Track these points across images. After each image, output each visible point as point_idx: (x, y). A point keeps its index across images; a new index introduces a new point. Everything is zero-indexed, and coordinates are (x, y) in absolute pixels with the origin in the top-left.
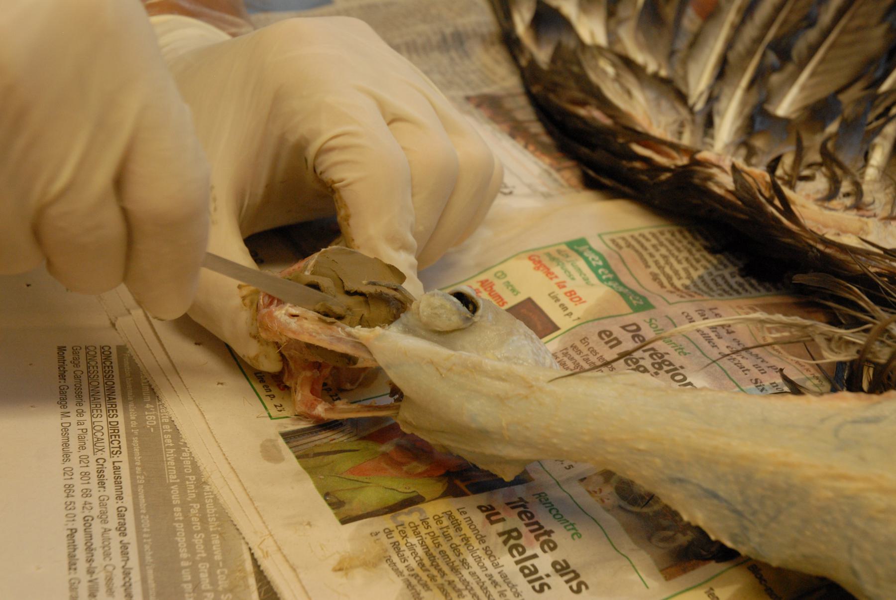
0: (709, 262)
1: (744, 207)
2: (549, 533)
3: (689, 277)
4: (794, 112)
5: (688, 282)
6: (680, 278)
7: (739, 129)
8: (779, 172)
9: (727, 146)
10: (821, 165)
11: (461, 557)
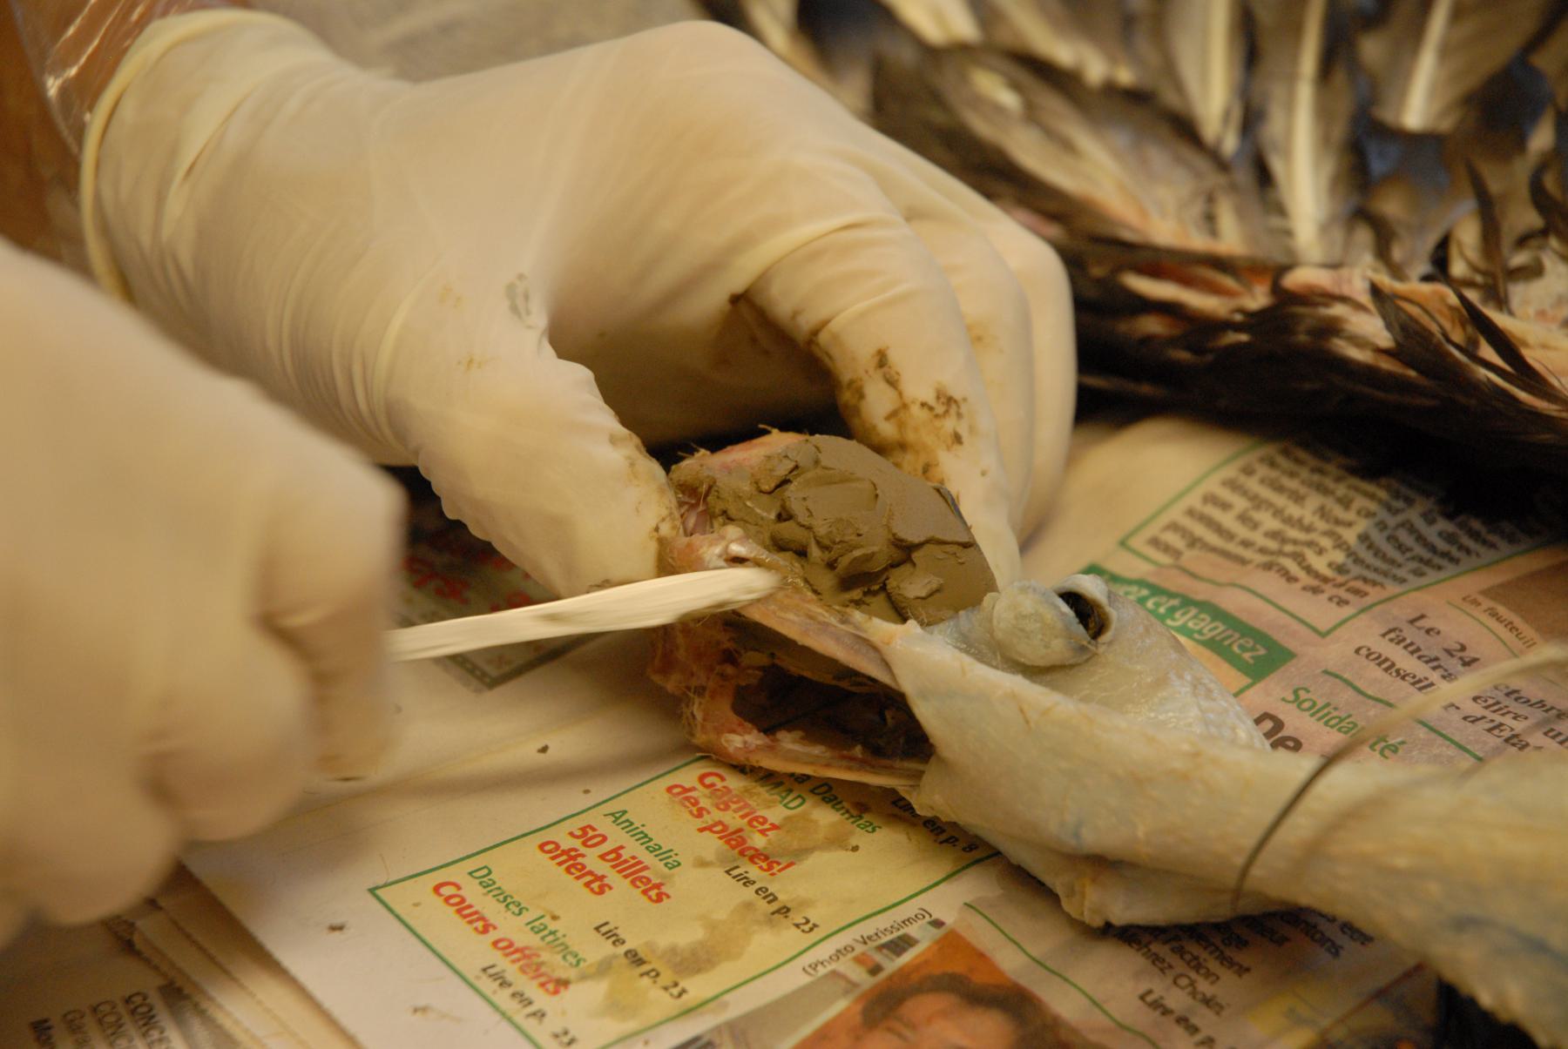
0: (1372, 497)
1: (1424, 382)
3: (1340, 544)
4: (1443, 113)
5: (1339, 557)
6: (1321, 552)
7: (1335, 182)
8: (1458, 268)
9: (1324, 229)
10: (1544, 233)
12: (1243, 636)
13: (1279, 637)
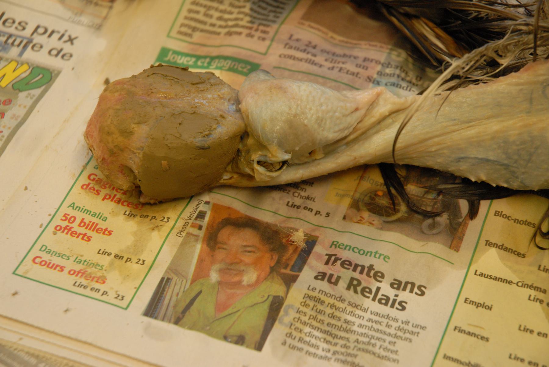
2: (371, 267)
3: (246, 15)
6: (242, 19)
11: (342, 320)
12: (239, 63)
13: (251, 60)
